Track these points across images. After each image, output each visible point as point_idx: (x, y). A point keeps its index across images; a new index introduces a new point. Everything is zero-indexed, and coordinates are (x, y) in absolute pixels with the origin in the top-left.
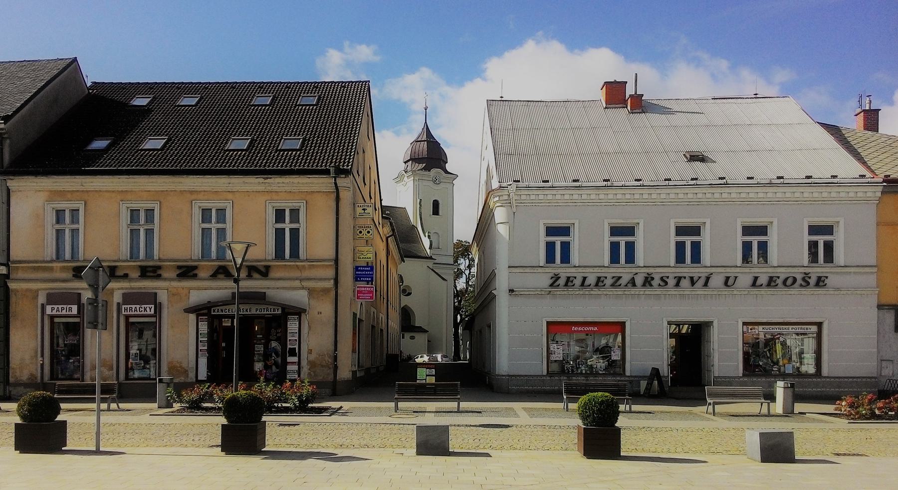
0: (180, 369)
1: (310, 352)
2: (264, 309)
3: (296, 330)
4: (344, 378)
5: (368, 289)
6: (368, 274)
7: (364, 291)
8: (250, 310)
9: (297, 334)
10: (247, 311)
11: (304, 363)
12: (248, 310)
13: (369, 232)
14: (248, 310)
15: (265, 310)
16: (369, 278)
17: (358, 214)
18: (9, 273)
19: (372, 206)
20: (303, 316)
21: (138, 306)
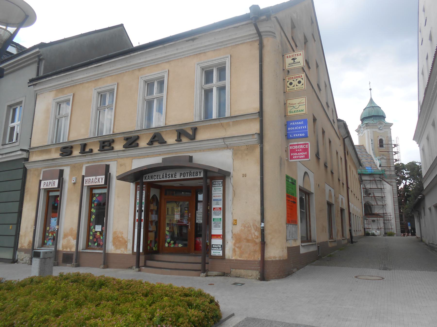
0: (121, 239)
1: (235, 223)
2: (187, 173)
3: (220, 196)
4: (275, 257)
5: (302, 146)
6: (300, 130)
7: (298, 149)
8: (175, 175)
9: (221, 202)
10: (172, 176)
11: (229, 237)
12: (174, 176)
13: (299, 82)
14: (174, 176)
15: (189, 174)
16: (302, 133)
17: (287, 65)
18: (29, 157)
19: (302, 54)
20: (227, 180)
21: (94, 177)
